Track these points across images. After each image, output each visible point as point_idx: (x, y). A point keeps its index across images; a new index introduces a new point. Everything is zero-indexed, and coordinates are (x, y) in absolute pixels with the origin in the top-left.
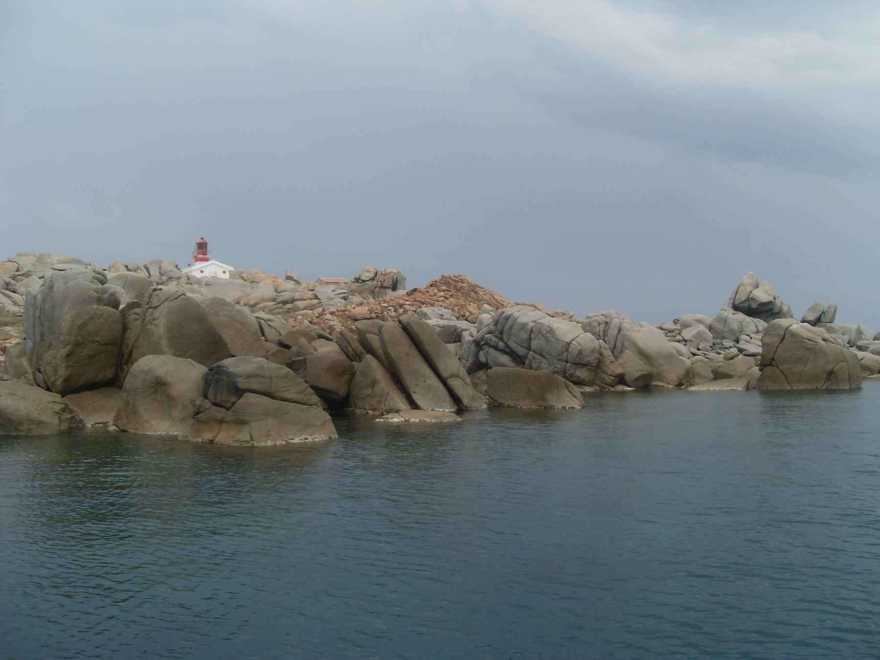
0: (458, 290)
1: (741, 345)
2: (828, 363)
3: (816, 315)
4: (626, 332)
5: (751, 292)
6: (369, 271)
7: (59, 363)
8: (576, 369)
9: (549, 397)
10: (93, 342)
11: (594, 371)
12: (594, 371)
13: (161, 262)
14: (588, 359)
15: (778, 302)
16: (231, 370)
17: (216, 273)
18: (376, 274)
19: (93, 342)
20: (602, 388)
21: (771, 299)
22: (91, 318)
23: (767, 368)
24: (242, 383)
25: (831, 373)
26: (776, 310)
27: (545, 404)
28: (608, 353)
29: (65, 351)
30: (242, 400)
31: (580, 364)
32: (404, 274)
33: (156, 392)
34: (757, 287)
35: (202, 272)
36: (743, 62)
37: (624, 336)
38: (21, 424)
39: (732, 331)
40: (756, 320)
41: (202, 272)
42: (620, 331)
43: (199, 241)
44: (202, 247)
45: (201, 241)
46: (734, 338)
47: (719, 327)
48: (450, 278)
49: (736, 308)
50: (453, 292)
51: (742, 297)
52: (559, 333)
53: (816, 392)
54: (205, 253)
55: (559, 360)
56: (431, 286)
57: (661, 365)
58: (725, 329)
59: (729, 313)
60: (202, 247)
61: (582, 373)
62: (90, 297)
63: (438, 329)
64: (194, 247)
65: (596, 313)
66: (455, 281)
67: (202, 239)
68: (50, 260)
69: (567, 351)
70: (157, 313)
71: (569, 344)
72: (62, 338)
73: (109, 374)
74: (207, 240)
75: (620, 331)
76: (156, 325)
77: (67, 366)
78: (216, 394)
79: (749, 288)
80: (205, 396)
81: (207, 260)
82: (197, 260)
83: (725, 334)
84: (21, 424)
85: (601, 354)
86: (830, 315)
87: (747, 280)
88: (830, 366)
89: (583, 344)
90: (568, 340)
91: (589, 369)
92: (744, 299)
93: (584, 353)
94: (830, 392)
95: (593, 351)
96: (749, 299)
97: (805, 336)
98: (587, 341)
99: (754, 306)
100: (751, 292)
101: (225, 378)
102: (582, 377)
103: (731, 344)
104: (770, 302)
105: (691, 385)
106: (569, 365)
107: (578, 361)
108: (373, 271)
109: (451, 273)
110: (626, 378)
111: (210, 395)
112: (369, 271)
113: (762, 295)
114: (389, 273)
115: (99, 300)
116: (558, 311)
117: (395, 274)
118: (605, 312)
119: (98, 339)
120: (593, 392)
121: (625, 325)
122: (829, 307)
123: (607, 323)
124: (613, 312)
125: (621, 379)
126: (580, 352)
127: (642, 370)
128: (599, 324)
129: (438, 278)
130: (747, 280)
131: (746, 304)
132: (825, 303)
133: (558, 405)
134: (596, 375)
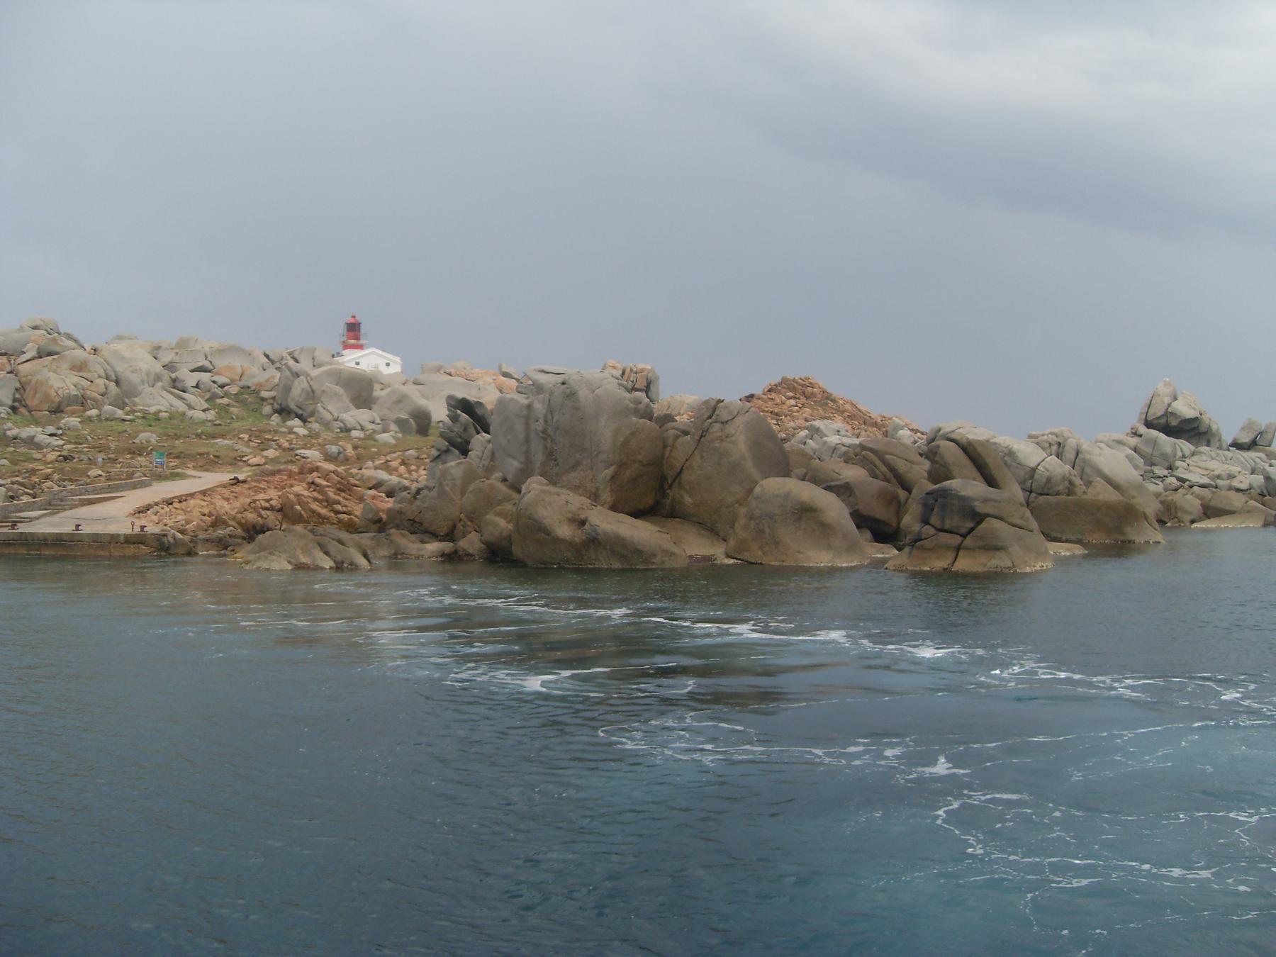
0: (807, 398)
1: (1177, 473)
3: (1252, 436)
4: (1087, 456)
5: (1169, 405)
6: (614, 367)
7: (602, 487)
9: (1128, 529)
10: (635, 461)
13: (314, 350)
16: (963, 493)
17: (376, 366)
19: (635, 461)
22: (633, 434)
24: (980, 508)
27: (1122, 538)
28: (1078, 481)
29: (609, 472)
30: (983, 526)
33: (800, 519)
34: (1175, 399)
35: (388, 365)
36: (1038, 74)
37: (1084, 461)
38: (654, 556)
39: (1164, 456)
40: (1179, 441)
41: (358, 363)
42: (1078, 454)
43: (350, 320)
44: (353, 328)
45: (352, 321)
46: (1167, 464)
48: (794, 380)
49: (1149, 425)
50: (803, 400)
51: (1157, 411)
52: (1021, 456)
54: (358, 338)
56: (769, 391)
59: (1142, 429)
60: (353, 328)
62: (627, 408)
64: (342, 329)
65: (1046, 429)
68: (198, 347)
69: (1032, 477)
70: (730, 429)
71: (1034, 470)
72: (604, 456)
73: (649, 500)
74: (360, 319)
75: (1078, 454)
76: (733, 443)
77: (612, 491)
78: (943, 519)
79: (1167, 400)
80: (926, 522)
81: (360, 347)
82: (346, 347)
83: (1155, 460)
84: (654, 556)
85: (1071, 482)
86: (1270, 436)
87: (1164, 390)
90: (1033, 464)
92: (1159, 414)
95: (1064, 478)
98: (1053, 466)
99: (1174, 423)
100: (1169, 405)
101: (955, 502)
103: (1166, 472)
106: (1033, 495)
109: (795, 374)
111: (934, 520)
112: (614, 367)
113: (1184, 409)
114: (642, 370)
115: (636, 411)
117: (649, 371)
118: (1056, 430)
119: (640, 457)
121: (1085, 447)
122: (1267, 426)
123: (1059, 444)
124: (1064, 429)
126: (1049, 480)
128: (1050, 445)
129: (777, 380)
130: (1164, 390)
131: (1163, 421)
133: (1139, 539)
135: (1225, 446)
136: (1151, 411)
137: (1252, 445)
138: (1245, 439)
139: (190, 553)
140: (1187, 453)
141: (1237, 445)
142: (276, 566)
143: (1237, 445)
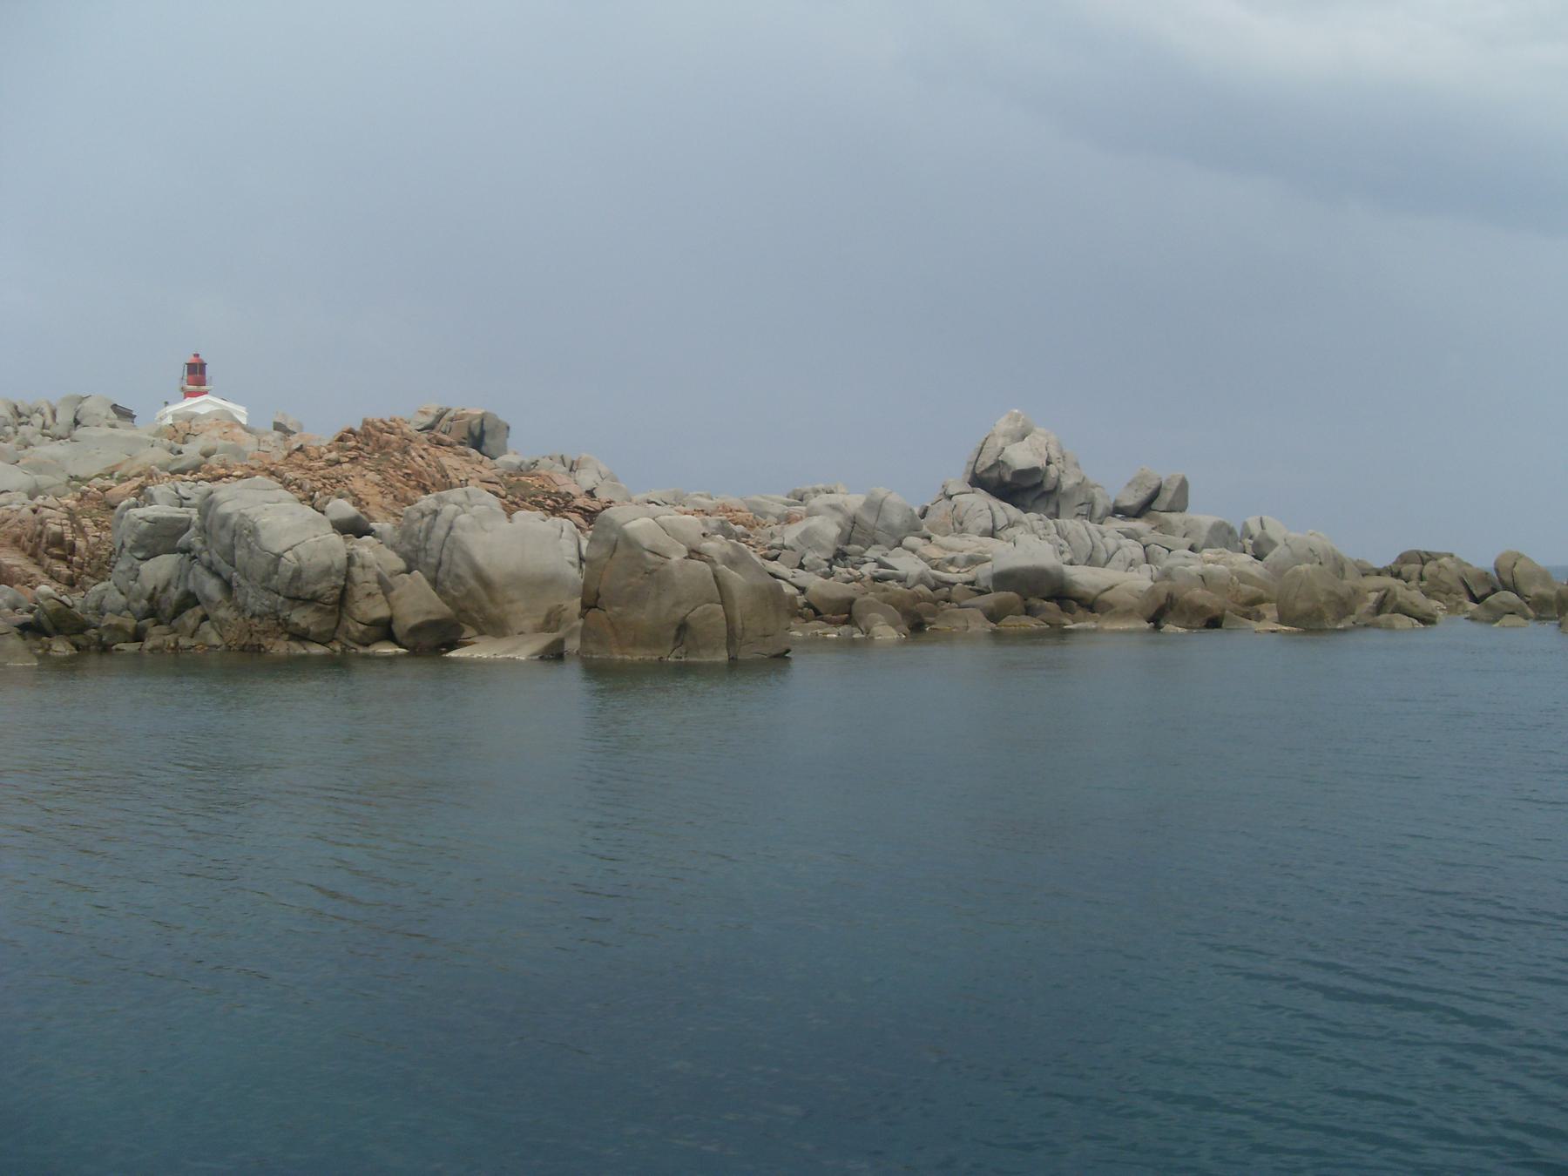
2: (678, 604)
3: (1142, 495)
8: (292, 608)
11: (332, 611)
12: (332, 611)
14: (312, 588)
15: (1053, 471)
18: (440, 417)
20: (345, 647)
21: (1041, 463)
23: (591, 613)
25: (683, 627)
26: (1048, 486)
31: (298, 598)
32: (503, 417)
37: (455, 541)
42: (451, 528)
43: (191, 359)
44: (197, 372)
47: (869, 519)
51: (987, 460)
53: (659, 669)
54: (202, 382)
55: (266, 589)
57: (511, 602)
58: (879, 525)
60: (197, 372)
61: (302, 617)
63: (145, 525)
64: (180, 371)
66: (381, 431)
67: (197, 355)
69: (276, 572)
71: (279, 556)
74: (204, 357)
75: (451, 528)
79: (1000, 442)
87: (1003, 424)
88: (681, 612)
89: (304, 557)
91: (319, 610)
92: (989, 463)
93: (304, 575)
94: (683, 670)
96: (999, 464)
97: (646, 543)
102: (303, 624)
104: (1035, 471)
105: (452, 646)
107: (293, 592)
108: (434, 411)
110: (396, 628)
113: (1022, 457)
116: (820, 486)
120: (325, 656)
125: (385, 630)
126: (297, 574)
127: (429, 613)
131: (995, 474)
132: (1164, 472)
134: (339, 622)
135: (1099, 511)
136: (981, 460)
137: (1143, 510)
138: (1131, 500)
139: (105, 649)
140: (1001, 521)
141: (1118, 511)
142: (719, 659)
143: (1118, 511)
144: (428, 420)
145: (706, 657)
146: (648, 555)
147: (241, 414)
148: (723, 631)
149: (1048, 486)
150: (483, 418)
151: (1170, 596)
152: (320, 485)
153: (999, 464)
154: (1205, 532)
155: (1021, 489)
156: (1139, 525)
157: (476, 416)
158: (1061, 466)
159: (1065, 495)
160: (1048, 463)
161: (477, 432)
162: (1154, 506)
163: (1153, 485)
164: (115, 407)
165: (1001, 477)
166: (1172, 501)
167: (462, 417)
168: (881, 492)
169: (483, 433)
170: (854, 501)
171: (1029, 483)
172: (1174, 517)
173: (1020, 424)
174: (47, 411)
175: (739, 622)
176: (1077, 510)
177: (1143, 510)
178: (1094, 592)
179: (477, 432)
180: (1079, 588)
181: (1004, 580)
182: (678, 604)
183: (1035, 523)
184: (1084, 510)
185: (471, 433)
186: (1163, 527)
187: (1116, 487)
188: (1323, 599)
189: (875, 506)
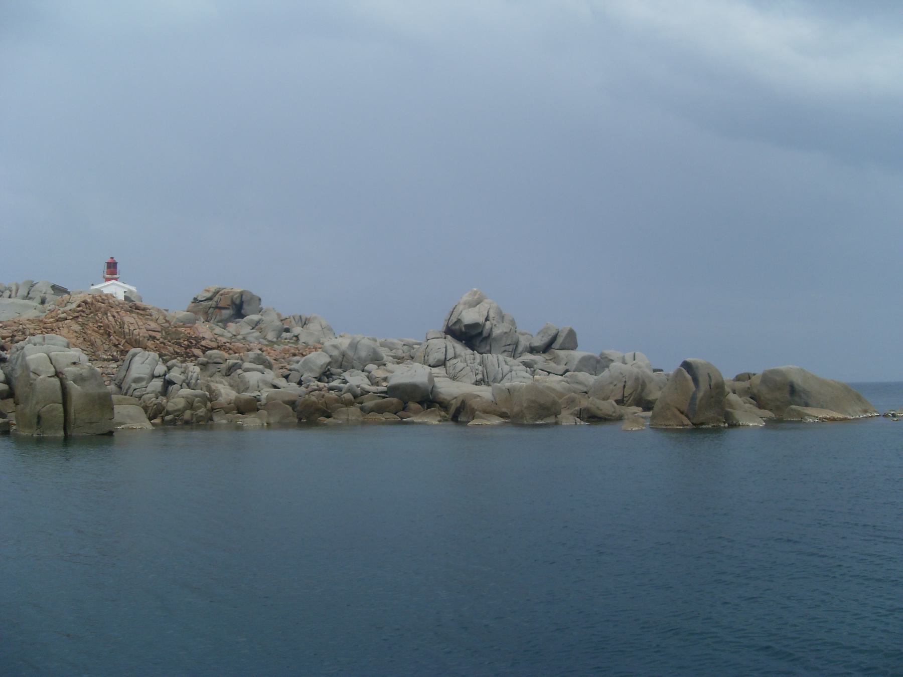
3: (546, 339)
18: (216, 293)
21: (481, 320)
26: (485, 334)
32: (256, 292)
43: (109, 260)
44: (112, 267)
47: (350, 353)
60: (112, 267)
64: (104, 267)
67: (112, 258)
74: (116, 259)
87: (466, 297)
88: (38, 407)
96: (459, 321)
104: (476, 325)
108: (213, 290)
113: (470, 316)
132: (561, 324)
135: (520, 349)
138: (538, 342)
141: (532, 350)
142: (58, 435)
143: (532, 350)
144: (208, 295)
145: (49, 434)
146: (31, 374)
147: (133, 289)
148: (62, 420)
149: (485, 334)
150: (241, 294)
151: (463, 402)
152: (39, 332)
153: (459, 321)
154: (576, 362)
155: (471, 336)
156: (538, 358)
157: (236, 293)
158: (494, 322)
159: (495, 339)
160: (487, 319)
161: (238, 302)
162: (553, 346)
163: (553, 332)
164: (54, 287)
165: (461, 330)
166: (563, 343)
167: (228, 293)
168: (358, 337)
169: (242, 302)
170: (344, 343)
171: (475, 332)
172: (562, 353)
173: (476, 297)
174: (14, 288)
175: (72, 414)
176: (504, 349)
177: (547, 348)
178: (449, 398)
179: (238, 302)
180: (441, 396)
181: (394, 390)
182: (37, 403)
183: (468, 357)
184: (510, 348)
185: (233, 303)
186: (556, 359)
187: (532, 332)
188: (525, 405)
189: (354, 346)
